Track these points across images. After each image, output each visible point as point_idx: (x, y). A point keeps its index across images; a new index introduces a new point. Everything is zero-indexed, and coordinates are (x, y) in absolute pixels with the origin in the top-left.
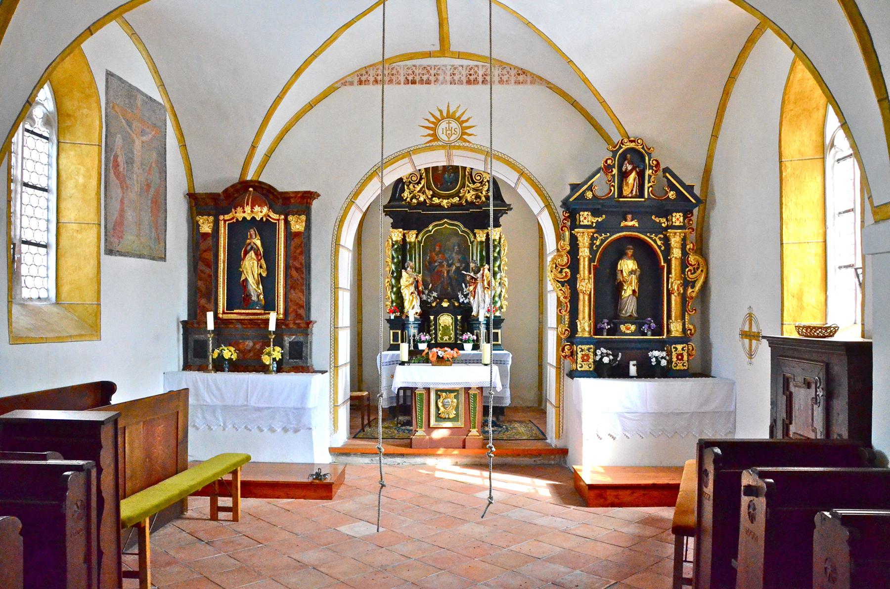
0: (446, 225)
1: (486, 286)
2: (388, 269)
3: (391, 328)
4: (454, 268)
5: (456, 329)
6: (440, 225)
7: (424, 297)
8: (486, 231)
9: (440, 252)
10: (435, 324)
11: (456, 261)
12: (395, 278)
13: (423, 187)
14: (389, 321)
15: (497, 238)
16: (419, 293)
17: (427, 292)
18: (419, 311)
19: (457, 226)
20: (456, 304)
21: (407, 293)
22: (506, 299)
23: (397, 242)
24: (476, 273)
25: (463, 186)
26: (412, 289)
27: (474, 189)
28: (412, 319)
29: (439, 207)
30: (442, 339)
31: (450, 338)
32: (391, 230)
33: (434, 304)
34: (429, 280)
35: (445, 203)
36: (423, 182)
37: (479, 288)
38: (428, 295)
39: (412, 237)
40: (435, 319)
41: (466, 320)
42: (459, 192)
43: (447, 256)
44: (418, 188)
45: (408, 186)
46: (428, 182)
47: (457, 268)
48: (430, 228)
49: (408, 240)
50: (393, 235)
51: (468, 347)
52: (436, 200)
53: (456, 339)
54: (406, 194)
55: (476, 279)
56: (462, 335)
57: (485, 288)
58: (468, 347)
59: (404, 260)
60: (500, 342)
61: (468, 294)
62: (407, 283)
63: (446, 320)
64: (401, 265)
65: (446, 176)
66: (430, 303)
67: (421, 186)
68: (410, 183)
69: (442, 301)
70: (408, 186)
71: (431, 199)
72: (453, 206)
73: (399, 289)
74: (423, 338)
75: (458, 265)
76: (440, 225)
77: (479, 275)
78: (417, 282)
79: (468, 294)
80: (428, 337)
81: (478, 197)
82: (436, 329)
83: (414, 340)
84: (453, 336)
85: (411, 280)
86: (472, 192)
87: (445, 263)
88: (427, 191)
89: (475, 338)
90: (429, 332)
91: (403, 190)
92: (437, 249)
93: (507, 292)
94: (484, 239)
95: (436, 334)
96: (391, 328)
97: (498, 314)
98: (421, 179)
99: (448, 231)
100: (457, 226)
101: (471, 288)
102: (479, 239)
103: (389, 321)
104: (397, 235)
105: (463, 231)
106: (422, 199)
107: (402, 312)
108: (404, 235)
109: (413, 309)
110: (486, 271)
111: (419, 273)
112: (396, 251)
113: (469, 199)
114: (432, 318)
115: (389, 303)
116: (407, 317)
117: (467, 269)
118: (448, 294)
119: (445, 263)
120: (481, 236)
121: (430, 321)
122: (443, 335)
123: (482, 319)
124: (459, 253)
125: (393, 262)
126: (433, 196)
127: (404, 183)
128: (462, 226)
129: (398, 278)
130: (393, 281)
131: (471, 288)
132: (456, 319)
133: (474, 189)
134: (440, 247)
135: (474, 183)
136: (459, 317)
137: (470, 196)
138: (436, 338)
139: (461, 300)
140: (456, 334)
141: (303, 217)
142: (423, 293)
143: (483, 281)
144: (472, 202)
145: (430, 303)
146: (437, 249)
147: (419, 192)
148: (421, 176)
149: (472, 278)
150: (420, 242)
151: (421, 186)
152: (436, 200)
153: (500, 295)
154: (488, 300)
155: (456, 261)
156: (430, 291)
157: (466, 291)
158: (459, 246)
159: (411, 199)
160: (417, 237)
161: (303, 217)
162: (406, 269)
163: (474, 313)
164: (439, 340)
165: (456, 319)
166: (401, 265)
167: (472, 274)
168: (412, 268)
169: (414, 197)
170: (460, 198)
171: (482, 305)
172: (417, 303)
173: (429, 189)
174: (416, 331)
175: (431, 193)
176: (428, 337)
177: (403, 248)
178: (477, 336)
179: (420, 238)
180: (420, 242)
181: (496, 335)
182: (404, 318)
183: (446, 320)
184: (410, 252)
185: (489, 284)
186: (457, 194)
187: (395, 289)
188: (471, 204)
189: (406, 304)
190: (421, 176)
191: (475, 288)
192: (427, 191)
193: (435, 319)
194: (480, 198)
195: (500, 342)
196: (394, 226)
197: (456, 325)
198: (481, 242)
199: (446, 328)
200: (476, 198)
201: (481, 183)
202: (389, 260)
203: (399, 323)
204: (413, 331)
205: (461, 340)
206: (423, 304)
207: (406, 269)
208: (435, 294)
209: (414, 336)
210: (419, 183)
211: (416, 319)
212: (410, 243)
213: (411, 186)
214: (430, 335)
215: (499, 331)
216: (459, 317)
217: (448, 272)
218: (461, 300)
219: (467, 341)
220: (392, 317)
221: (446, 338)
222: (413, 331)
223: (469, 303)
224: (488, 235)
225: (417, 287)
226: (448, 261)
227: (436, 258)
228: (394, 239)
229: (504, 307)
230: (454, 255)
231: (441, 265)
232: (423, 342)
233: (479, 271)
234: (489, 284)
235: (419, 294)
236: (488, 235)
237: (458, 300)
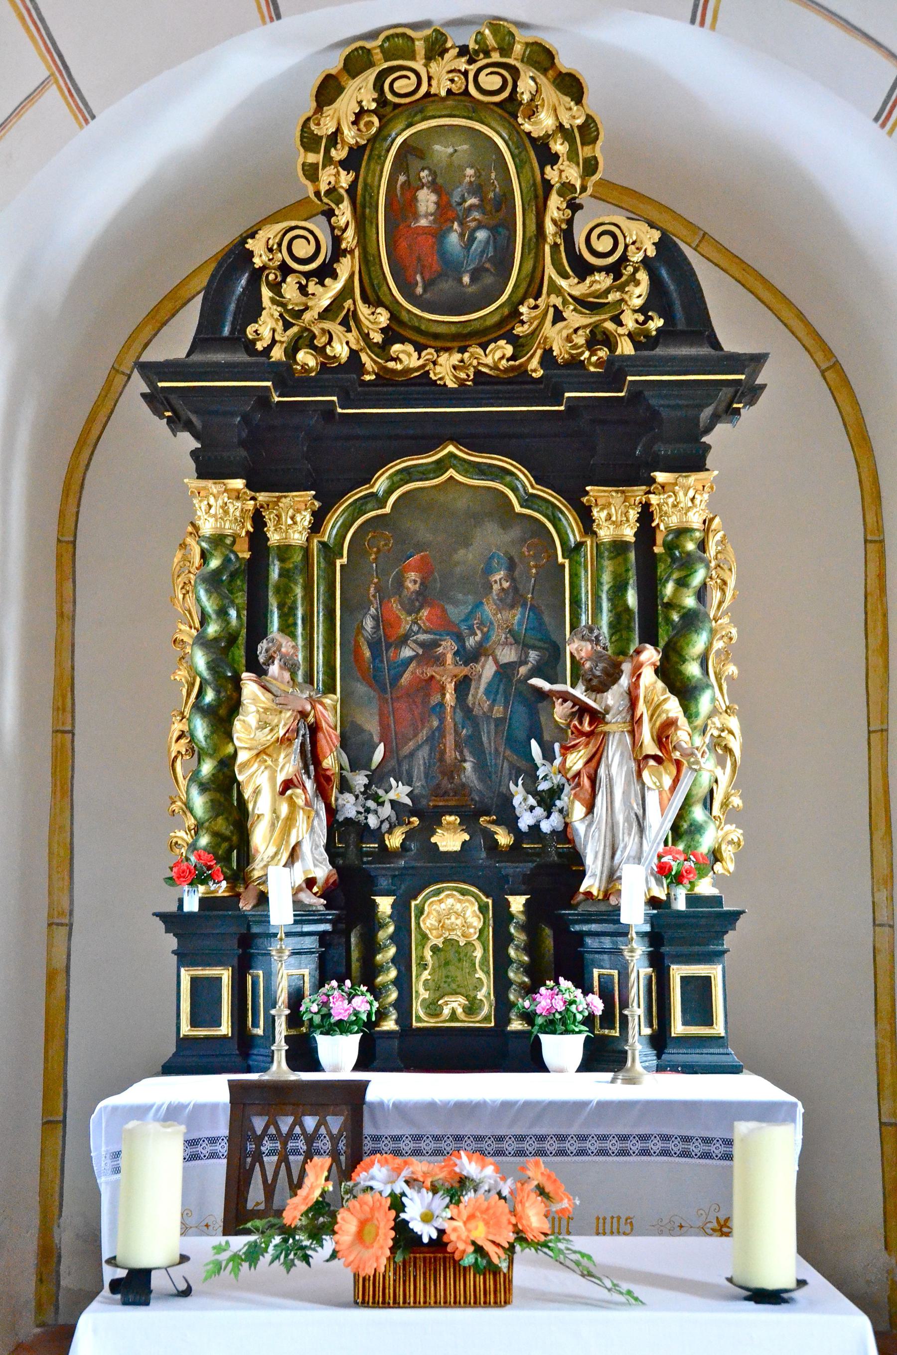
0: (456, 471)
1: (650, 748)
2: (182, 675)
3: (184, 957)
4: (488, 670)
5: (502, 962)
6: (423, 473)
7: (349, 806)
8: (638, 493)
9: (423, 598)
10: (402, 938)
11: (499, 635)
12: (208, 712)
13: (347, 292)
14: (175, 921)
15: (695, 520)
16: (323, 783)
17: (360, 780)
18: (322, 871)
19: (502, 474)
20: (504, 838)
21: (259, 783)
22: (732, 815)
23: (217, 540)
24: (598, 687)
25: (533, 287)
26: (289, 764)
27: (583, 304)
28: (281, 913)
29: (422, 386)
30: (433, 1008)
31: (471, 1009)
32: (193, 483)
33: (395, 841)
34: (371, 725)
35: (446, 368)
36: (345, 268)
37: (616, 764)
38: (368, 793)
39: (292, 520)
40: (401, 913)
41: (552, 910)
42: (515, 315)
43: (455, 613)
44: (324, 295)
45: (276, 287)
46: (368, 261)
47: (505, 671)
48: (380, 484)
49: (274, 538)
50: (200, 506)
51: (563, 1050)
52: (406, 357)
53: (503, 1007)
54: (266, 328)
55: (597, 717)
56: (531, 990)
57: (641, 761)
58: (563, 1050)
59: (257, 629)
60: (719, 1028)
61: (556, 792)
62: (265, 737)
63: (453, 914)
64: (236, 655)
65: (453, 238)
66: (378, 835)
67: (335, 287)
68: (285, 270)
69: (431, 820)
70: (276, 287)
71: (382, 349)
72: (484, 385)
73: (227, 764)
74: (340, 1009)
75: (508, 655)
76: (423, 473)
77: (613, 698)
78: (314, 729)
79: (556, 792)
80: (363, 1004)
81: (599, 338)
82: (403, 960)
83: (294, 1019)
84: (485, 993)
85: (284, 722)
86: (575, 318)
87: (448, 647)
88: (364, 310)
89: (597, 1005)
90: (369, 976)
91: (251, 310)
92: (412, 581)
93: (739, 781)
94: (629, 533)
95: (404, 983)
96: (184, 957)
97: (705, 887)
98: (338, 253)
99: (462, 503)
100: (502, 474)
101: (576, 761)
102: (605, 533)
103: (175, 921)
104: (219, 508)
105: (529, 501)
106: (340, 350)
107: (239, 876)
108: (258, 519)
109: (289, 868)
110: (648, 677)
111: (330, 688)
112: (213, 581)
113: (559, 350)
114: (385, 904)
115: (183, 836)
116: (263, 899)
117: (550, 667)
118: (462, 789)
119: (448, 647)
120: (615, 516)
121: (371, 923)
122: (440, 990)
123: (634, 913)
124: (513, 597)
125: (202, 641)
126: (391, 335)
127: (257, 274)
128: (524, 477)
129: (223, 715)
130: (201, 729)
131: (576, 761)
132: (502, 916)
133: (583, 304)
134: (426, 570)
135: (583, 270)
136: (517, 903)
137: (558, 339)
138: (404, 1006)
139: (525, 821)
140: (502, 985)
141: (742, 1128)
142: (345, 786)
143: (634, 724)
144: (575, 363)
145: (378, 835)
146: (412, 581)
147: (326, 314)
148: (336, 241)
149: (582, 710)
150: (330, 552)
151: (335, 287)
152: (406, 357)
153: (708, 801)
154: (659, 823)
155: (499, 635)
156: (378, 778)
157: (548, 775)
158: (511, 566)
159: (292, 350)
160: (316, 527)
161: (742, 1128)
162: (258, 670)
163: (591, 884)
164: (421, 1018)
165: (502, 916)
166: (236, 655)
167: (579, 692)
168: (290, 667)
169: (305, 340)
170: (520, 345)
171: (628, 843)
172: (311, 834)
173: (373, 299)
174: (306, 970)
175: (383, 318)
176: (363, 1004)
177: (248, 575)
178: (606, 995)
179: (330, 531)
180: (330, 552)
181: (698, 994)
182: (246, 905)
183: (453, 914)
184: (284, 591)
185: (663, 736)
186: (504, 327)
187: (207, 768)
188: (563, 372)
189: (261, 838)
190: (336, 241)
191: (595, 759)
192: (364, 310)
193: (401, 913)
194: (609, 341)
195: (719, 1028)
196: (209, 467)
197: (502, 940)
198: (619, 547)
199: (451, 954)
200: (592, 344)
201: (615, 270)
202: (187, 633)
203: (224, 933)
204: (287, 969)
205: (528, 1017)
206: (343, 836)
207: (258, 670)
208: (400, 792)
209: (296, 999)
210: (326, 272)
211: (303, 914)
212: (284, 551)
213: (290, 290)
214: (376, 992)
215: (715, 972)
216: (517, 903)
217: (463, 685)
218: (525, 821)
219: (558, 1024)
220: (191, 905)
221: (454, 1004)
222: (287, 969)
223: (564, 834)
224: (646, 515)
225: (311, 757)
226: (460, 638)
227: (406, 623)
228: (208, 527)
229: (728, 852)
230: (489, 609)
231: (429, 653)
232: (342, 1027)
233: (612, 676)
234: (663, 736)
235: (322, 791)
236: (646, 515)
237: (509, 820)
